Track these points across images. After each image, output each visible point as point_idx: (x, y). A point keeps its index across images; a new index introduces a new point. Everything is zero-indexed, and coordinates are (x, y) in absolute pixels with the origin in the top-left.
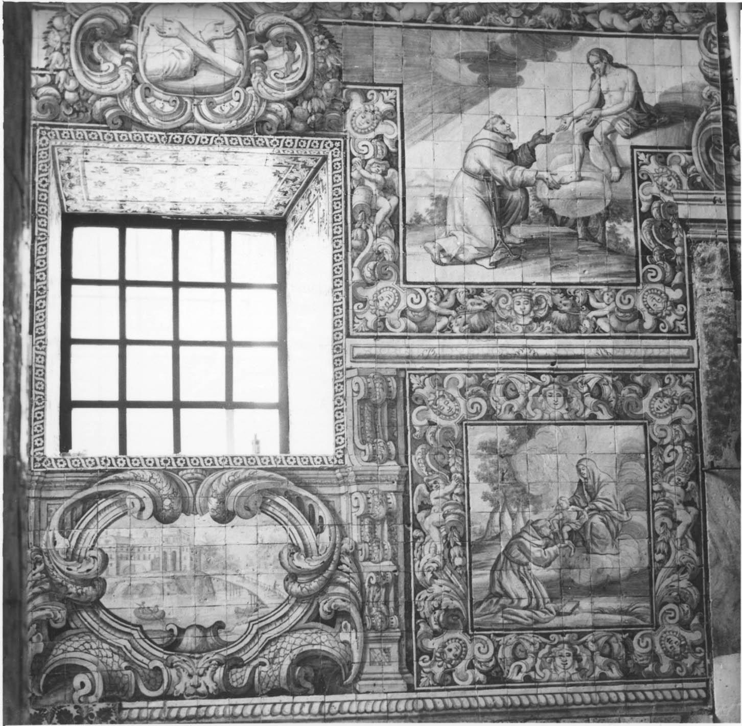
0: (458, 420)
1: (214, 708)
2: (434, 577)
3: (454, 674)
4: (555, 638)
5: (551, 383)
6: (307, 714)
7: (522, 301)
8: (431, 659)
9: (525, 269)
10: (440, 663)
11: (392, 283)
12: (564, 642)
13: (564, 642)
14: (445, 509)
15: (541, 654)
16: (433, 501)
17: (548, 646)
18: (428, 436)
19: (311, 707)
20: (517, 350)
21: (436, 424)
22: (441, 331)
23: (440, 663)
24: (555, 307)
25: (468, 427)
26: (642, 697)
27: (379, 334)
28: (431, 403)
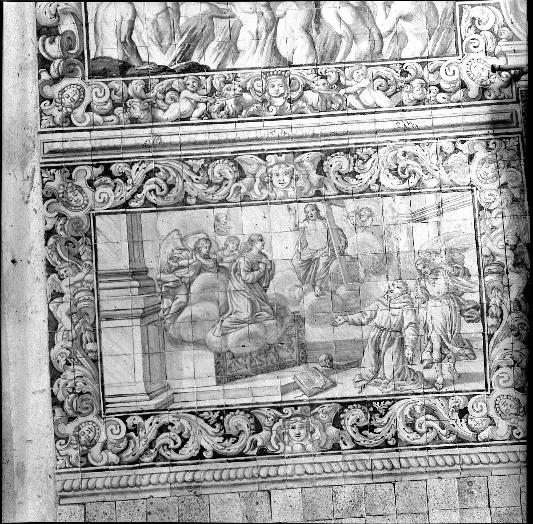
0: (87, 210)
1: (93, 480)
2: (68, 364)
3: (89, 456)
4: (289, 411)
5: (277, 163)
6: (85, 490)
7: (276, 84)
8: (66, 442)
9: (197, 61)
10: (75, 446)
11: (77, 80)
12: (297, 415)
13: (297, 415)
14: (77, 297)
15: (274, 428)
16: (66, 290)
17: (281, 420)
18: (58, 228)
19: (128, 479)
20: (145, 139)
21: (64, 216)
22: (200, 117)
23: (75, 446)
24: (307, 88)
25: (97, 218)
26: (475, 460)
27: (65, 129)
28: (61, 195)
